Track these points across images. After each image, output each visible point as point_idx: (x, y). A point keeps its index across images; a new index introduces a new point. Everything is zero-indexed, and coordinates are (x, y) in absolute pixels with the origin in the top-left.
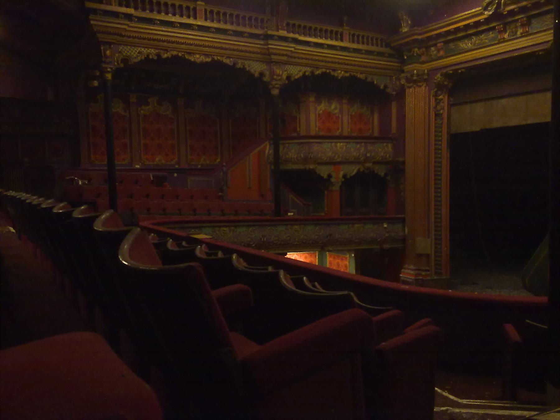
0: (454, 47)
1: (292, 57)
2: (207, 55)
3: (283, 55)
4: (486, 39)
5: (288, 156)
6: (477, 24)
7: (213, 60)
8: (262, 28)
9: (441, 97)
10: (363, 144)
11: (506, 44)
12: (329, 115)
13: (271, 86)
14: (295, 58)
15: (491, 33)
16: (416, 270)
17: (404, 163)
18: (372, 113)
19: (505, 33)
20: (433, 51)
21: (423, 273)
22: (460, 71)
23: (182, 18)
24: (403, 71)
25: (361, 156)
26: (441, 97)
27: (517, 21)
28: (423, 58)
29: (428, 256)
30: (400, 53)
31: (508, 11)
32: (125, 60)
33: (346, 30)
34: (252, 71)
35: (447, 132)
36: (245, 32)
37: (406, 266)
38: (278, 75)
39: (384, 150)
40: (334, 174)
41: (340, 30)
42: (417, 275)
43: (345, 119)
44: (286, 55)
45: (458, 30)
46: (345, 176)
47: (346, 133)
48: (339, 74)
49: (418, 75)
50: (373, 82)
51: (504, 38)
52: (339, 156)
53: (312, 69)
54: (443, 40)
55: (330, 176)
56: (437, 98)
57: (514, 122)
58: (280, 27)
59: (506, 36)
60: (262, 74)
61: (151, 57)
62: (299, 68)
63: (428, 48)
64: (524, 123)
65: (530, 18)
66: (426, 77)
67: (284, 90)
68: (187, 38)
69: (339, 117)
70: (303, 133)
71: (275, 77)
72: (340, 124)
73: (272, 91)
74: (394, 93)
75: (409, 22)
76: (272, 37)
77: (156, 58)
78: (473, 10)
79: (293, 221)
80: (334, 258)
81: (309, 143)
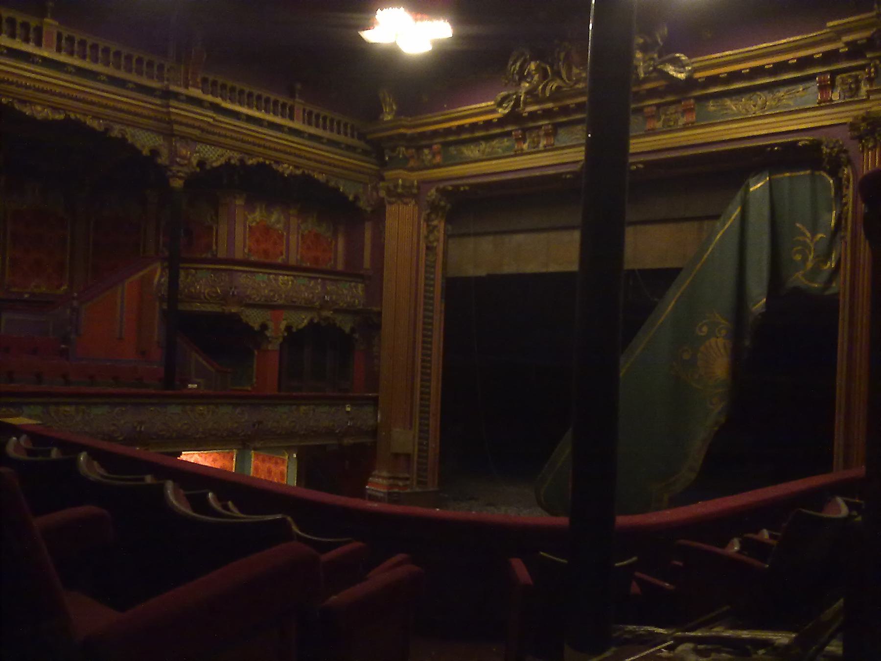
0: (455, 152)
2: (55, 109)
3: (193, 127)
6: (488, 124)
7: (68, 118)
8: (161, 79)
9: (435, 223)
10: (320, 280)
12: (267, 230)
13: (169, 173)
14: (214, 134)
15: (506, 140)
16: (390, 478)
17: (379, 314)
21: (401, 483)
24: (382, 179)
26: (435, 223)
27: (539, 127)
28: (412, 163)
29: (408, 456)
30: (380, 151)
31: (530, 113)
33: (299, 104)
34: (138, 146)
37: (376, 472)
39: (351, 293)
40: (271, 325)
41: (290, 102)
42: (391, 486)
44: (199, 128)
45: (461, 129)
46: (288, 328)
47: (292, 261)
48: (286, 169)
49: (403, 186)
50: (338, 189)
51: (522, 150)
52: (280, 295)
55: (264, 327)
57: (532, 268)
58: (191, 83)
59: (525, 146)
60: (155, 152)
62: (220, 151)
63: (419, 149)
64: (544, 270)
65: (557, 126)
66: (415, 191)
67: (192, 181)
69: (282, 235)
70: (221, 254)
71: (178, 160)
73: (171, 180)
74: (369, 209)
75: (394, 107)
76: (176, 96)
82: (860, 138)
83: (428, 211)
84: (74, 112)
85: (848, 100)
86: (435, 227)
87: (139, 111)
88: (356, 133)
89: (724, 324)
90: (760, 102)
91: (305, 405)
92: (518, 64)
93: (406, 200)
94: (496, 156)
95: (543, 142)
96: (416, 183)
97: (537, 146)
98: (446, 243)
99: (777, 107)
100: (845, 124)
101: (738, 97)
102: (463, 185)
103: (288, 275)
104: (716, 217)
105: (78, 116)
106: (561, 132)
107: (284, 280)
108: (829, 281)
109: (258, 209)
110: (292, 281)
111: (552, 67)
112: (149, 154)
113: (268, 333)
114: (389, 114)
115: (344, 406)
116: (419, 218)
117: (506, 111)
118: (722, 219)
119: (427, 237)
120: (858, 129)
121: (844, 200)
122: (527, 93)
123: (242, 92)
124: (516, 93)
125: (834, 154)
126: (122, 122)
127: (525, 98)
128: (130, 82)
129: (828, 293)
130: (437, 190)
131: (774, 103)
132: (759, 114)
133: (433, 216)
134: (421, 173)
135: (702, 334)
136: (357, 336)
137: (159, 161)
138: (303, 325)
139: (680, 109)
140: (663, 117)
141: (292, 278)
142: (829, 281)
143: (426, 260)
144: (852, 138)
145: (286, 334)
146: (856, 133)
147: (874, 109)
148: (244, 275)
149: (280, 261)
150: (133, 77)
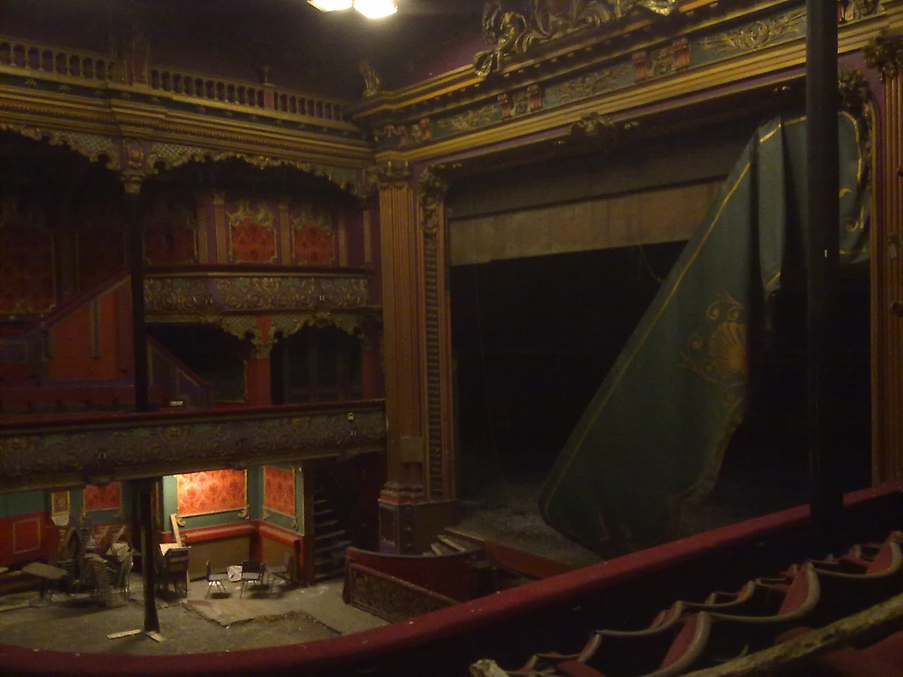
0: (444, 126)
1: (164, 130)
3: (144, 126)
4: (487, 116)
5: (169, 301)
6: (471, 91)
8: (100, 77)
9: (433, 207)
10: (313, 280)
11: (512, 125)
12: (254, 229)
13: (123, 179)
14: (171, 131)
15: (492, 107)
16: (401, 490)
17: (380, 312)
18: (335, 227)
19: (512, 108)
20: (416, 132)
21: (413, 495)
22: (454, 166)
24: (374, 163)
25: (308, 301)
26: (433, 207)
27: (525, 88)
28: (403, 142)
29: (420, 465)
30: (368, 130)
31: (512, 73)
32: (160, 164)
33: (268, 87)
34: (83, 152)
35: (445, 264)
36: (63, 84)
37: (388, 484)
38: (136, 160)
39: (351, 290)
40: (258, 332)
41: (257, 88)
42: (402, 499)
43: (285, 235)
44: (151, 126)
45: (445, 99)
46: (278, 334)
47: (286, 262)
48: (262, 161)
49: (394, 169)
50: (326, 178)
51: (510, 116)
52: (266, 300)
53: (207, 151)
54: (428, 113)
55: (249, 335)
56: (426, 207)
57: (534, 251)
58: (134, 78)
59: (513, 112)
60: (104, 158)
62: (181, 149)
63: (409, 125)
64: (547, 252)
65: (543, 86)
66: (406, 173)
67: (148, 184)
69: (273, 233)
70: (204, 260)
71: (130, 163)
72: (275, 246)
73: (126, 186)
74: (364, 197)
75: (378, 81)
76: (117, 94)
77: (204, 161)
78: (462, 69)
79: (180, 417)
80: (274, 475)
81: (207, 277)
82: (880, 64)
83: (424, 194)
85: (864, 18)
86: (433, 211)
87: (80, 114)
88: (341, 115)
89: (737, 306)
90: (761, 33)
91: (299, 416)
92: (493, 18)
93: (398, 184)
94: (482, 126)
95: (531, 106)
96: (407, 164)
97: (525, 111)
98: (447, 228)
99: (781, 37)
100: (859, 50)
101: (736, 30)
102: (455, 162)
103: (274, 277)
104: (723, 178)
105: (11, 126)
106: (548, 91)
107: (269, 284)
108: (858, 246)
109: (241, 208)
110: (280, 283)
111: (527, 17)
112: (96, 160)
113: (255, 342)
114: (372, 90)
115: (346, 413)
116: (415, 201)
117: (486, 74)
118: (729, 179)
119: (424, 224)
120: (873, 55)
121: (868, 145)
122: (503, 51)
123: (199, 82)
124: (492, 52)
125: (851, 89)
126: (64, 128)
127: (502, 56)
129: (858, 260)
130: (430, 170)
131: (777, 33)
132: (759, 48)
133: (430, 199)
134: (411, 153)
135: (713, 318)
136: (362, 336)
137: (110, 166)
138: (296, 330)
139: (672, 52)
140: (655, 63)
141: (280, 280)
142: (858, 246)
143: (425, 249)
144: (870, 66)
145: (276, 341)
146: (873, 60)
147: (893, 26)
148: (222, 281)
149: (271, 261)
150: (68, 79)
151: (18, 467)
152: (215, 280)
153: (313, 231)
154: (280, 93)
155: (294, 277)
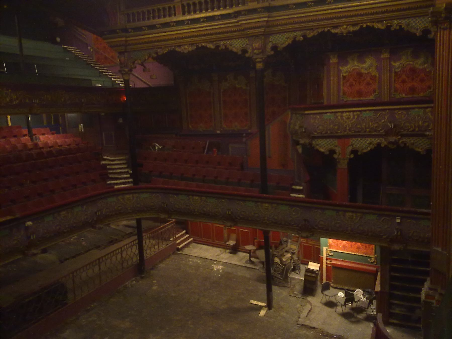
2: (354, 25)
7: (198, 48)
14: (277, 25)
23: (171, 18)
40: (338, 150)
55: (332, 152)
60: (244, 51)
61: (297, 39)
62: (286, 35)
68: (203, 30)
77: (302, 38)
84: (364, 23)
105: (203, 44)
128: (242, 11)
151: (196, 210)
152: (396, 111)
153: (413, 71)
154: (185, 3)
155: (370, 110)
